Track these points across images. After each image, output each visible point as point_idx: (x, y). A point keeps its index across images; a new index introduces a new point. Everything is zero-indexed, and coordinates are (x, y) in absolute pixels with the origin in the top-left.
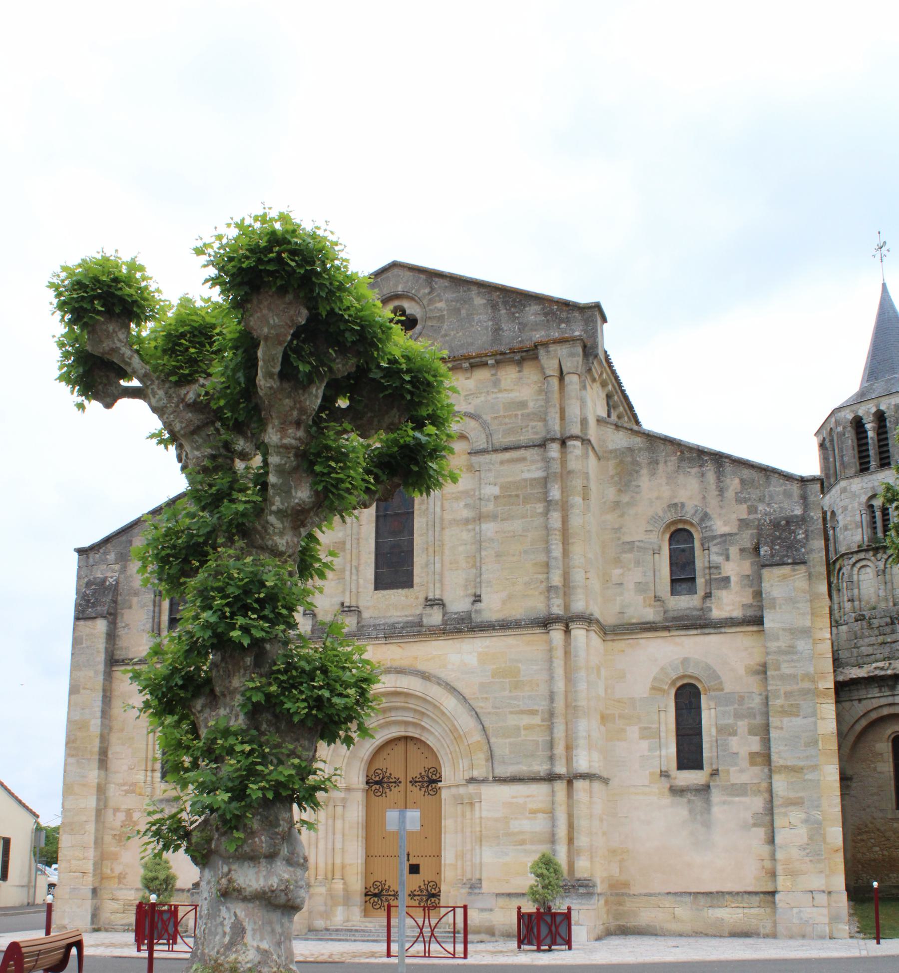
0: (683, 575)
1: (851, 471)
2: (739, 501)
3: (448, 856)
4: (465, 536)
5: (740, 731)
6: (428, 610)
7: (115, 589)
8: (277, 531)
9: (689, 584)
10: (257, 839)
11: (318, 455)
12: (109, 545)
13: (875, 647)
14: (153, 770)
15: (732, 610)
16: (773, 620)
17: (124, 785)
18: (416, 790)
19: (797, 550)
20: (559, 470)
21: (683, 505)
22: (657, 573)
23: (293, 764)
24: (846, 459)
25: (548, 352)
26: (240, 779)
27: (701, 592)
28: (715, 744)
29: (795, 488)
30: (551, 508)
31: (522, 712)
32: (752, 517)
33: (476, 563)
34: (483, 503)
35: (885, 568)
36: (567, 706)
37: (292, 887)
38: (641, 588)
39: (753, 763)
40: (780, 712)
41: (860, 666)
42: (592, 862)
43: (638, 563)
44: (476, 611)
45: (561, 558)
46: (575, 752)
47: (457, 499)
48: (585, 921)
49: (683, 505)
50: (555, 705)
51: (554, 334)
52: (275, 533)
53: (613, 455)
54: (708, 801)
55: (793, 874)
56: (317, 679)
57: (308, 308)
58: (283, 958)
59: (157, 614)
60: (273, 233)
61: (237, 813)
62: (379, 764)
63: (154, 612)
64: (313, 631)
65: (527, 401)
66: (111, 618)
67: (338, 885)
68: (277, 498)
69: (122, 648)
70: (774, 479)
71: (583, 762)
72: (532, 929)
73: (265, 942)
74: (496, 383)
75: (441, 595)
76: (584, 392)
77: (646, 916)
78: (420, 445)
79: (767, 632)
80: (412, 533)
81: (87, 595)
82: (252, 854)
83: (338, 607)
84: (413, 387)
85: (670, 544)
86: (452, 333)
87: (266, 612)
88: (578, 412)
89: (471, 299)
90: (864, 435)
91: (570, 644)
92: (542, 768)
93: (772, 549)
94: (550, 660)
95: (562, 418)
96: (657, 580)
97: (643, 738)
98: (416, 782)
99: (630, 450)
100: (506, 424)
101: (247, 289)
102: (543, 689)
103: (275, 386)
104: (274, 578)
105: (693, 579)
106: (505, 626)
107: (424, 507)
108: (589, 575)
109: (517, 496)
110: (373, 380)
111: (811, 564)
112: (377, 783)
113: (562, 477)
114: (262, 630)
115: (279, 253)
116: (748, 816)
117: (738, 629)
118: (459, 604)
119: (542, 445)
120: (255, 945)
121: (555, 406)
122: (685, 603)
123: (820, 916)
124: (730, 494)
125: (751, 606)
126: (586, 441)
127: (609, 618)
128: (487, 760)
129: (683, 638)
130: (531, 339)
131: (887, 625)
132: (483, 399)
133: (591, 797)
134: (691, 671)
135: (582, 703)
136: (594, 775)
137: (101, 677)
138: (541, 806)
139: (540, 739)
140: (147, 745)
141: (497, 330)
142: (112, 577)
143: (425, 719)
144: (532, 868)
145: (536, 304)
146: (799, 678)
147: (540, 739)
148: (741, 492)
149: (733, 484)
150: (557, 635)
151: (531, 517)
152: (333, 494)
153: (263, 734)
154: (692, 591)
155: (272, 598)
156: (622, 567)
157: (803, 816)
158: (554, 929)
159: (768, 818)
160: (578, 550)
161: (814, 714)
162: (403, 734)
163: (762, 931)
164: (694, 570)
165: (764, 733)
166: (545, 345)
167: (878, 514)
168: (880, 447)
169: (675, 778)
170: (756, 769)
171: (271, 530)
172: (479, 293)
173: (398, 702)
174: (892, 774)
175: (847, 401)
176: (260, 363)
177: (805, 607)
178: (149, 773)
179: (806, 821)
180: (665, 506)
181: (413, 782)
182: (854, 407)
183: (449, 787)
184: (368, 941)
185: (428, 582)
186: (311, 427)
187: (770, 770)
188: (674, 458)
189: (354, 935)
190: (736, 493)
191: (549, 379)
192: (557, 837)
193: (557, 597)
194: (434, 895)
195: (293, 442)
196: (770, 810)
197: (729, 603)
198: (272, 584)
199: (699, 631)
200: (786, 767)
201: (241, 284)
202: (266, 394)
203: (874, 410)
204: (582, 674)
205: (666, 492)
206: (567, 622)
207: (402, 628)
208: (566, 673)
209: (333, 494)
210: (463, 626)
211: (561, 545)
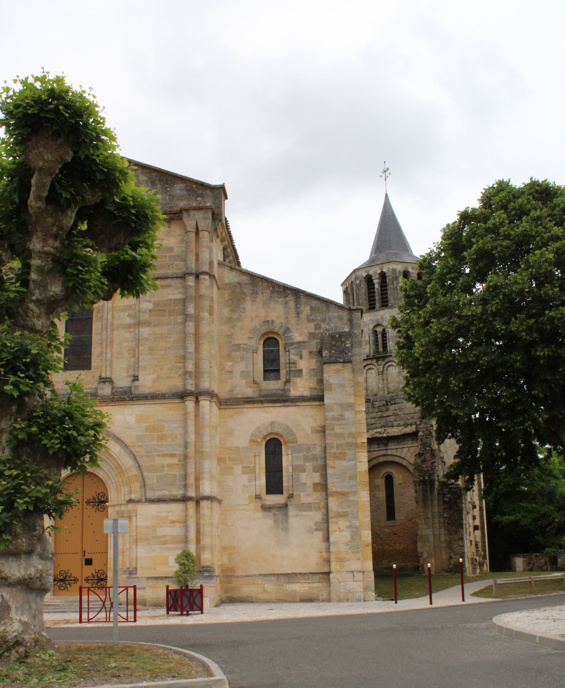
0: (271, 368)
2: (309, 321)
4: (128, 335)
6: (102, 385)
8: (35, 315)
9: (276, 374)
10: (19, 540)
11: (70, 261)
13: (376, 419)
16: (330, 398)
18: (90, 508)
20: (194, 294)
21: (273, 322)
22: (255, 366)
23: (48, 485)
24: (361, 301)
25: (189, 215)
26: (8, 496)
27: (283, 379)
28: (291, 478)
30: (188, 319)
32: (317, 331)
33: (135, 354)
34: (141, 314)
35: (383, 370)
36: (196, 452)
37: (44, 575)
38: (244, 375)
39: (315, 490)
43: (242, 358)
44: (135, 387)
45: (193, 353)
47: (123, 310)
50: (188, 451)
51: (204, 201)
52: (33, 317)
54: (286, 515)
55: (341, 560)
56: (66, 423)
57: (73, 151)
58: (37, 628)
60: (52, 90)
61: (7, 521)
68: (37, 291)
70: (332, 308)
71: (207, 489)
72: (177, 601)
73: (25, 616)
75: (111, 375)
76: (212, 244)
77: (246, 590)
78: (135, 260)
79: (326, 405)
80: (91, 332)
82: (15, 551)
84: (136, 218)
85: (264, 347)
87: (30, 373)
88: (208, 257)
90: (372, 287)
91: (199, 410)
92: (178, 492)
93: (330, 352)
94: (185, 421)
95: (197, 260)
96: (255, 370)
97: (244, 473)
99: (240, 284)
101: (29, 130)
102: (180, 440)
103: (42, 207)
104: (37, 348)
105: (278, 371)
106: (154, 397)
107: (100, 315)
108: (212, 365)
109: (164, 310)
110: (109, 211)
111: (354, 363)
113: (195, 299)
114: (27, 386)
115: (57, 106)
117: (307, 404)
119: (183, 277)
120: (18, 619)
122: (272, 385)
123: (357, 587)
124: (304, 316)
125: (315, 389)
126: (212, 276)
127: (223, 394)
128: (141, 488)
130: (177, 206)
131: (384, 405)
133: (212, 512)
134: (276, 430)
135: (207, 450)
139: (177, 473)
144: (176, 559)
145: (181, 183)
146: (346, 436)
147: (177, 473)
148: (311, 315)
149: (306, 310)
151: (174, 325)
152: (79, 290)
153: (24, 463)
154: (278, 378)
155: (34, 363)
157: (347, 523)
158: (191, 600)
160: (206, 349)
161: (355, 459)
163: (321, 598)
164: (279, 365)
166: (187, 210)
167: (380, 336)
168: (382, 295)
169: (265, 500)
170: (317, 494)
171: (30, 314)
172: (143, 173)
174: (385, 498)
175: (362, 265)
176: (33, 189)
177: (350, 390)
179: (349, 527)
181: (88, 502)
182: (367, 269)
183: (114, 506)
184: (58, 612)
185: (101, 366)
186: (65, 240)
187: (327, 495)
189: (47, 609)
190: (308, 316)
191: (189, 233)
192: (189, 539)
193: (191, 379)
194: (102, 580)
195: (52, 250)
196: (326, 520)
197: (301, 387)
198: (36, 352)
199: (282, 404)
200: (337, 492)
201: (24, 126)
202: (35, 212)
203: (379, 271)
204: (207, 430)
205: (262, 313)
206: (197, 395)
208: (195, 429)
209: (79, 290)
211: (194, 344)
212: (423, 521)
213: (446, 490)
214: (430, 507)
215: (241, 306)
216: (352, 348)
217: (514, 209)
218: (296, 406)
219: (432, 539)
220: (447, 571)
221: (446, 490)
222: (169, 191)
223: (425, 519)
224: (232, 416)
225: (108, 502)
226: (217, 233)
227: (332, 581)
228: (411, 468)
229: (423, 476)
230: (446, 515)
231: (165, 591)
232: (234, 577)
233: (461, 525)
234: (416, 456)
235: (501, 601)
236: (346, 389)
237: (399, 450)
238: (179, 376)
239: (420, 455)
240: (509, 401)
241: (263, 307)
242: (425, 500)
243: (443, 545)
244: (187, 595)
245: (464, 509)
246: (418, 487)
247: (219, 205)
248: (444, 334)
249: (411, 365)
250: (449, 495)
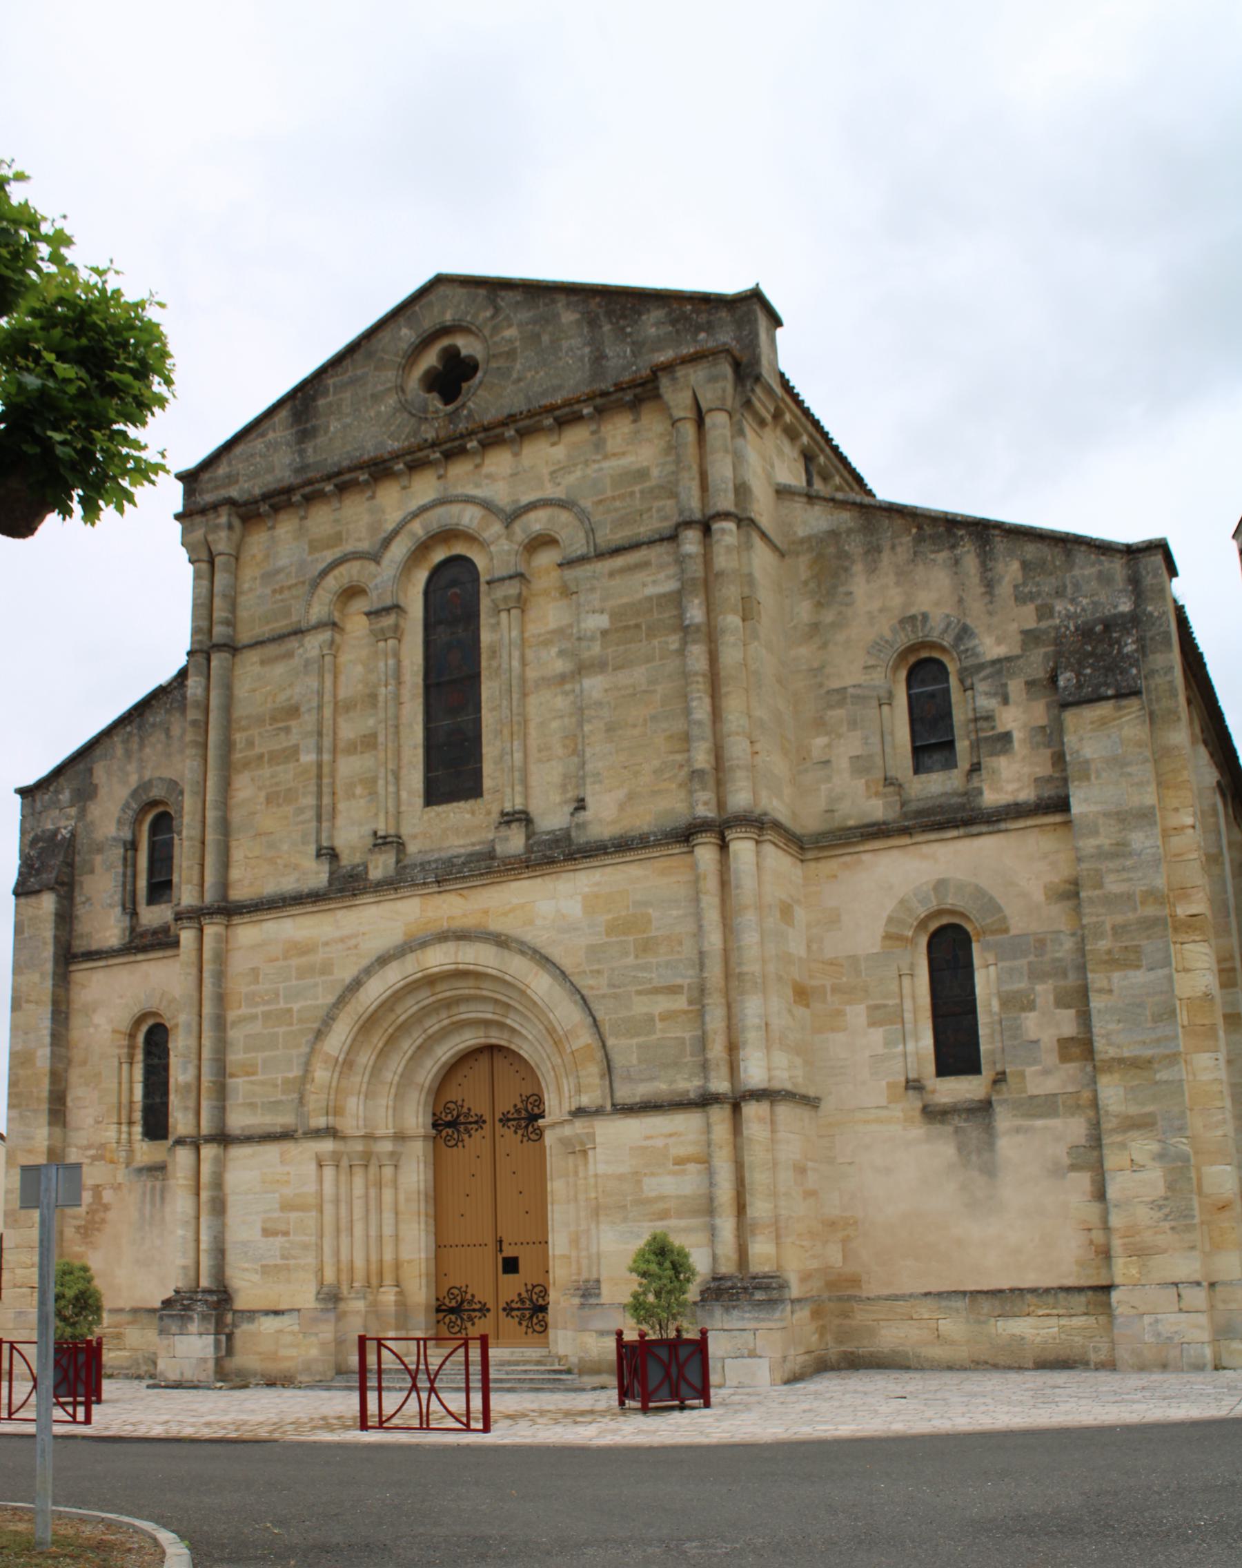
0: (932, 740)
2: (1021, 599)
3: (558, 1243)
4: (561, 703)
5: (1040, 1001)
6: (504, 831)
7: (70, 844)
12: (61, 780)
14: (131, 1123)
15: (1018, 790)
16: (1086, 800)
17: (89, 1147)
18: (508, 1132)
21: (925, 617)
22: (888, 738)
27: (964, 763)
29: (1117, 567)
30: (689, 639)
31: (656, 991)
33: (576, 745)
36: (727, 975)
38: (860, 765)
39: (1065, 1057)
40: (1106, 962)
43: (853, 724)
44: (578, 826)
46: (742, 1054)
47: (546, 643)
49: (925, 617)
50: (705, 975)
53: (805, 546)
54: (989, 1130)
55: (1141, 1253)
59: (129, 879)
62: (453, 1093)
63: (125, 875)
64: (331, 882)
65: (648, 468)
66: (63, 890)
67: (389, 1296)
69: (81, 936)
70: (1080, 555)
71: (755, 1073)
74: (599, 446)
75: (526, 805)
76: (740, 441)
77: (892, 1335)
81: (31, 858)
83: (370, 841)
86: (529, 375)
88: (729, 473)
89: (557, 316)
92: (688, 1085)
93: (1078, 674)
96: (888, 750)
97: (873, 1024)
98: (509, 1120)
99: (834, 534)
100: (616, 510)
102: (688, 950)
105: (950, 745)
106: (624, 846)
107: (495, 664)
109: (638, 626)
116: (1060, 1152)
117: (1030, 822)
119: (672, 538)
121: (690, 468)
122: (937, 785)
124: (1005, 589)
125: (1050, 779)
126: (745, 522)
128: (602, 1077)
129: (936, 846)
132: (578, 474)
133: (773, 1131)
134: (950, 901)
136: (778, 1092)
137: (49, 983)
138: (690, 1150)
139: (687, 1035)
140: (120, 1083)
141: (599, 358)
142: (65, 828)
143: (512, 1015)
146: (1138, 899)
147: (687, 1035)
148: (1024, 584)
149: (1010, 571)
150: (706, 854)
151: (661, 659)
154: (950, 764)
156: (827, 734)
157: (1155, 1147)
158: (674, 1371)
159: (1091, 1158)
161: (1167, 963)
162: (483, 1041)
163: (1093, 1357)
165: (1078, 999)
169: (933, 1092)
170: (1072, 1067)
172: (568, 305)
173: (464, 988)
178: (124, 1128)
179: (1161, 1156)
180: (895, 621)
188: (907, 539)
190: (1016, 587)
191: (679, 424)
192: (716, 1204)
193: (704, 789)
196: (1096, 1141)
197: (1011, 779)
199: (962, 831)
200: (1121, 1061)
204: (749, 917)
205: (896, 598)
206: (721, 829)
210: (559, 853)
215: (841, 589)
216: (1144, 655)
218: (999, 831)
222: (630, 334)
224: (835, 876)
225: (543, 1117)
226: (756, 414)
227: (1117, 1312)
232: (859, 1299)
236: (1129, 770)
238: (680, 785)
241: (898, 584)
244: (660, 1359)
247: (751, 341)
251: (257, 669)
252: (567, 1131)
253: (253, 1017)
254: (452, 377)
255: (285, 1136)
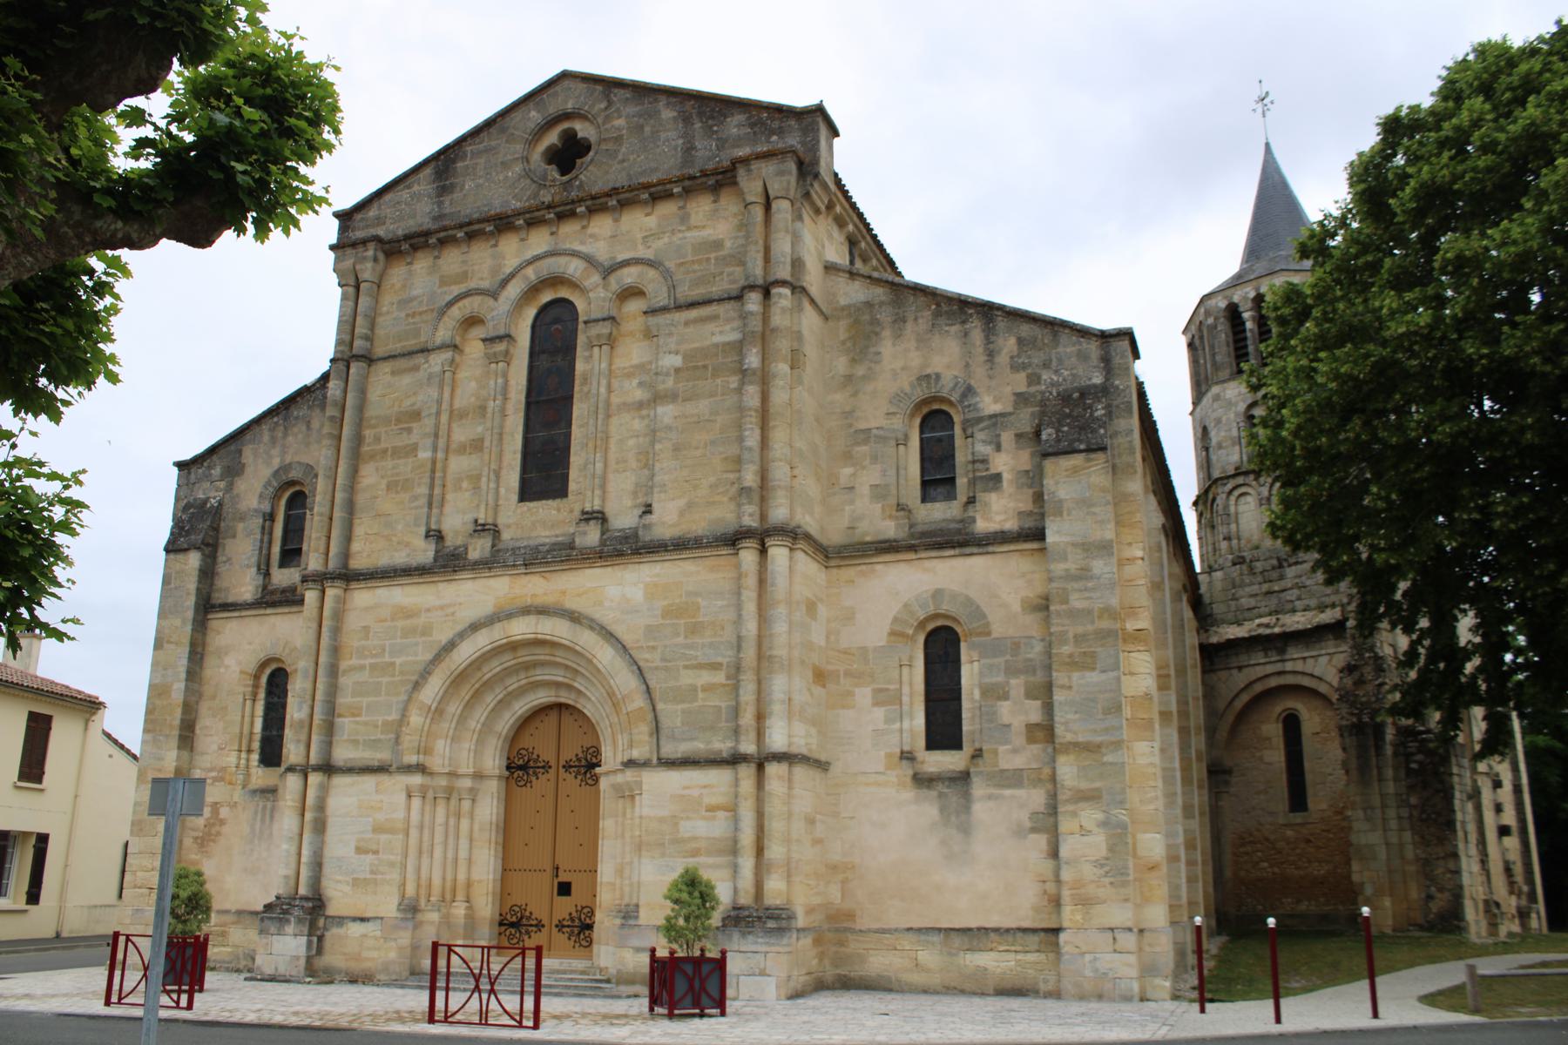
0: (938, 476)
1: (1225, 374)
2: (1015, 368)
4: (637, 425)
5: (1013, 693)
12: (215, 458)
14: (249, 751)
18: (570, 777)
19: (1094, 431)
21: (938, 376)
22: (902, 472)
24: (1218, 358)
25: (749, 171)
27: (962, 496)
29: (1093, 348)
31: (700, 666)
32: (1033, 389)
33: (647, 460)
36: (760, 657)
38: (878, 492)
39: (1031, 739)
41: (1240, 625)
42: (789, 882)
43: (875, 459)
45: (758, 450)
46: (768, 723)
47: (629, 376)
48: (755, 970)
54: (967, 796)
55: (1085, 902)
62: (527, 742)
63: (262, 541)
64: (435, 560)
67: (459, 910)
69: (220, 590)
74: (684, 219)
76: (798, 224)
77: (879, 962)
83: (471, 527)
85: (922, 432)
88: (787, 248)
92: (722, 746)
93: (1058, 431)
94: (738, 593)
96: (902, 481)
97: (876, 704)
99: (869, 304)
102: (729, 634)
105: (952, 481)
106: (681, 545)
107: (585, 389)
109: (705, 367)
112: (520, 768)
116: (1023, 817)
117: (1012, 547)
118: (623, 518)
119: (739, 298)
122: (939, 512)
123: (1125, 967)
124: (1003, 359)
125: (1030, 513)
126: (798, 289)
127: (834, 536)
128: (651, 735)
132: (666, 240)
133: (790, 788)
134: (945, 607)
136: (796, 756)
139: (723, 705)
141: (689, 149)
143: (579, 679)
147: (723, 705)
148: (1019, 356)
149: (1008, 344)
150: (748, 556)
154: (951, 496)
157: (1100, 816)
158: (697, 983)
159: (1048, 822)
162: (553, 699)
173: (542, 655)
174: (1283, 765)
178: (244, 755)
179: (1104, 824)
182: (1228, 293)
196: (1053, 809)
197: (999, 511)
199: (957, 551)
200: (1076, 745)
203: (1252, 294)
204: (781, 610)
205: (915, 360)
206: (762, 537)
207: (548, 551)
212: (1360, 813)
213: (1413, 746)
214: (1376, 784)
215: (872, 350)
217: (1510, 88)
219: (1382, 853)
220: (1421, 928)
221: (1413, 746)
223: (1365, 809)
226: (813, 204)
228: (1335, 697)
229: (1359, 716)
230: (1413, 800)
231: (647, 960)
233: (1450, 824)
234: (1341, 671)
235: (1481, 1026)
237: (1310, 662)
239: (1349, 669)
240: (1513, 526)
241: (917, 349)
242: (1363, 768)
243: (1412, 868)
244: (685, 973)
245: (1457, 787)
246: (1347, 740)
248: (1345, 382)
249: (1281, 461)
250: (1419, 757)
251: (388, 378)
252: (619, 778)
253: (362, 668)
254: (569, 154)
255: (381, 769)
